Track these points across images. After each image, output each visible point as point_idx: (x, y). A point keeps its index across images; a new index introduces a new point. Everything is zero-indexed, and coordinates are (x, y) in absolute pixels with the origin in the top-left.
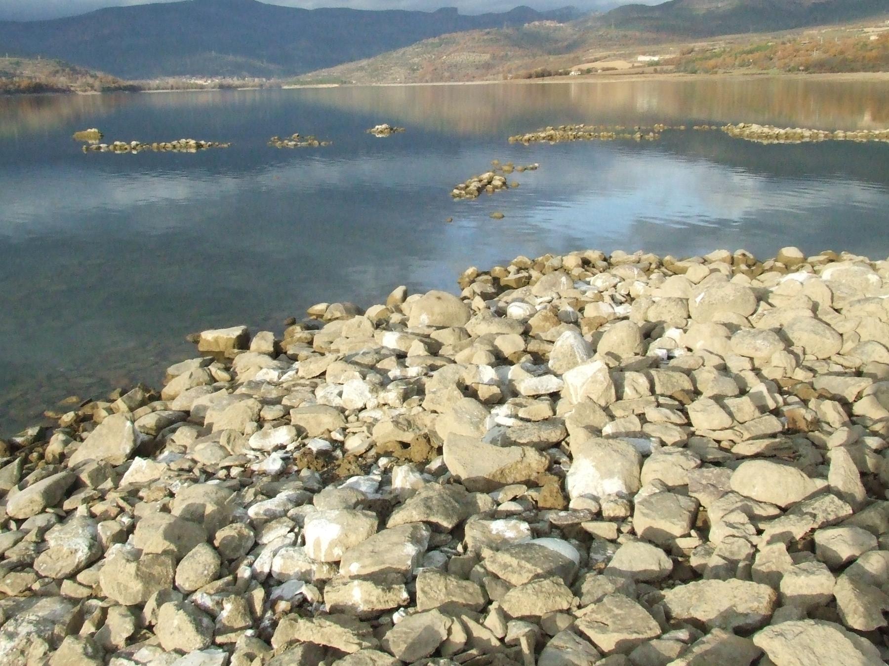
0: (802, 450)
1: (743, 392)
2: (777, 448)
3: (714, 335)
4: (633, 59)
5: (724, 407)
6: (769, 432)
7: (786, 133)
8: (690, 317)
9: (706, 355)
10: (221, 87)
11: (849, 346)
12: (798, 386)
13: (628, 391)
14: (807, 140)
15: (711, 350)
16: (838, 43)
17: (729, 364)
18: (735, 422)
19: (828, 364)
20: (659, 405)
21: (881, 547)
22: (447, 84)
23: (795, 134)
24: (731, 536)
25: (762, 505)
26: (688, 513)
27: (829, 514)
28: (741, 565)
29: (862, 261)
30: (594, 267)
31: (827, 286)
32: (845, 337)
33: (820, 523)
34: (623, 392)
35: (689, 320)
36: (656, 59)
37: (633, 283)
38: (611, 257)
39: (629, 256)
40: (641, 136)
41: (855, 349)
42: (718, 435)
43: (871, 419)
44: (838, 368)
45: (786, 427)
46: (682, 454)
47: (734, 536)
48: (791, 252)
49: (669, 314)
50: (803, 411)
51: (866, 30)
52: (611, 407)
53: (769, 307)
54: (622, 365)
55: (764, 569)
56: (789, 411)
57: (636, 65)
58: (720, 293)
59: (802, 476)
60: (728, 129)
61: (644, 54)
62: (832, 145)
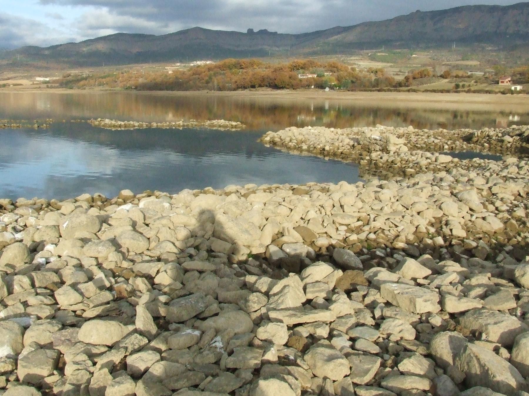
0: (124, 310)
1: (90, 278)
2: (109, 310)
3: (74, 246)
4: (33, 79)
5: (77, 290)
6: (105, 301)
7: (125, 124)
8: (61, 236)
9: (69, 259)
11: (153, 244)
12: (124, 271)
13: (17, 288)
14: (137, 128)
15: (72, 255)
16: (152, 74)
17: (83, 263)
18: (85, 298)
19: (142, 256)
20: (37, 294)
21: (162, 359)
23: (130, 124)
24: (77, 370)
25: (97, 347)
26: (52, 360)
27: (135, 345)
28: (82, 387)
29: (165, 195)
30: (5, 209)
31: (142, 212)
32: (151, 240)
33: (130, 351)
34: (13, 289)
35: (60, 238)
36: (47, 79)
37: (28, 218)
38: (16, 202)
39: (29, 201)
40: (38, 127)
41: (156, 246)
42: (74, 308)
43: (164, 285)
44: (147, 258)
45: (116, 297)
46: (49, 323)
47: (79, 370)
48: (127, 193)
49: (49, 235)
50: (125, 286)
51: (166, 68)
52: (5, 300)
53: (108, 226)
54: (16, 271)
55: (96, 386)
56: (117, 287)
57: (35, 82)
58: (78, 220)
59: (120, 325)
60: (92, 122)
61: (40, 76)
62: (149, 131)
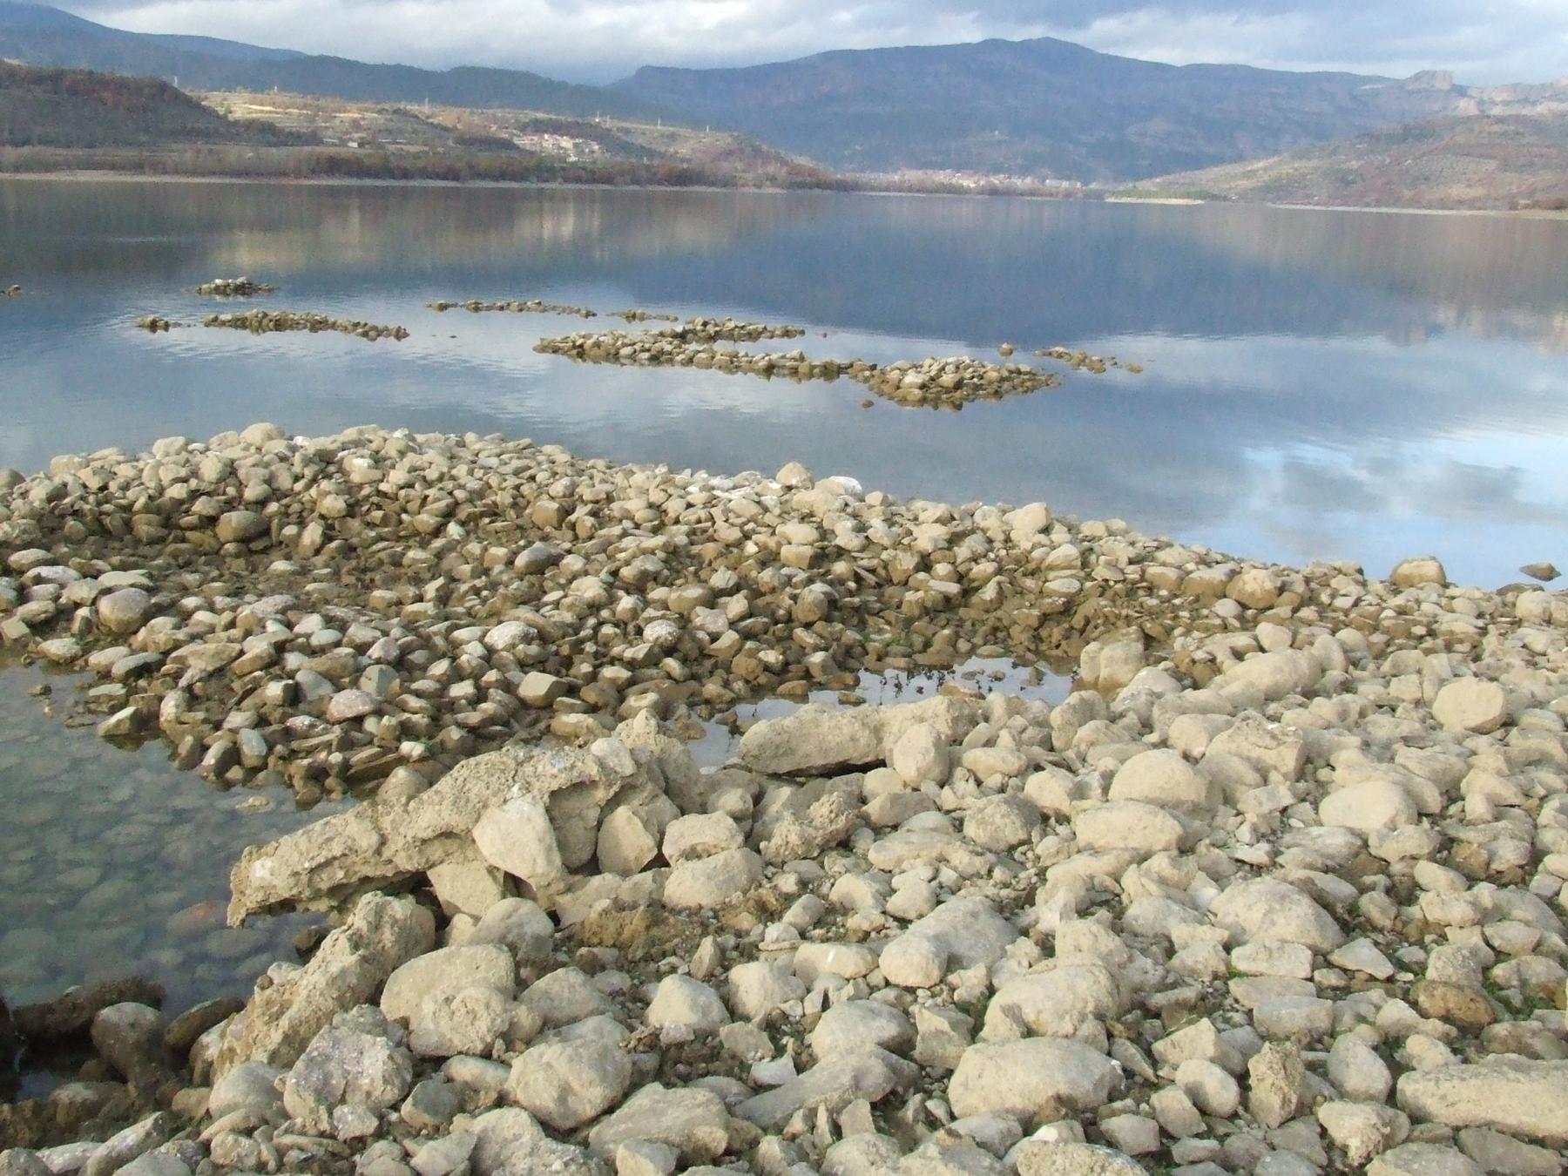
10: (993, 192)
22: (1405, 211)
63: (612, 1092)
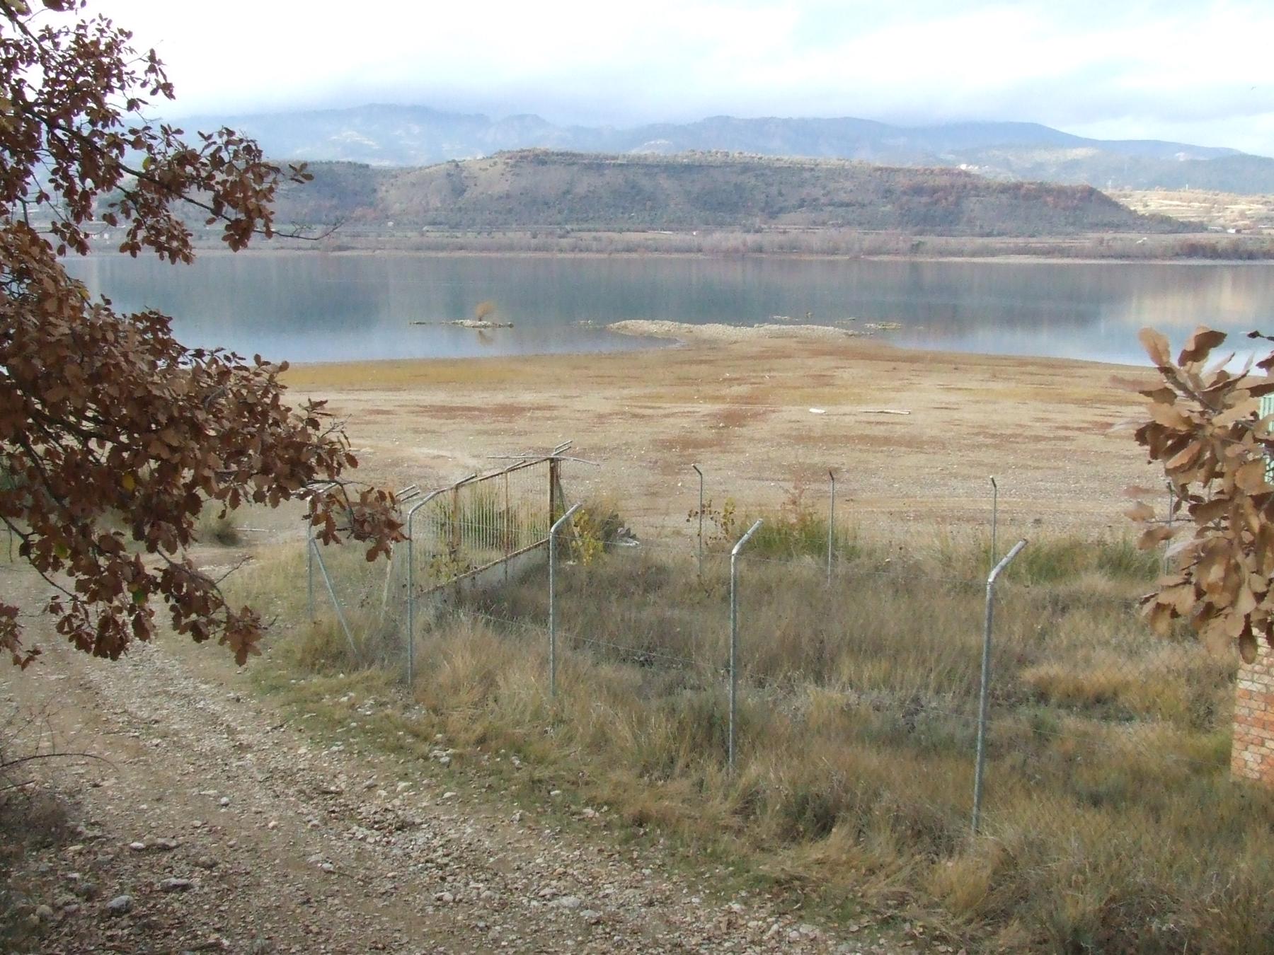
63: (737, 699)
